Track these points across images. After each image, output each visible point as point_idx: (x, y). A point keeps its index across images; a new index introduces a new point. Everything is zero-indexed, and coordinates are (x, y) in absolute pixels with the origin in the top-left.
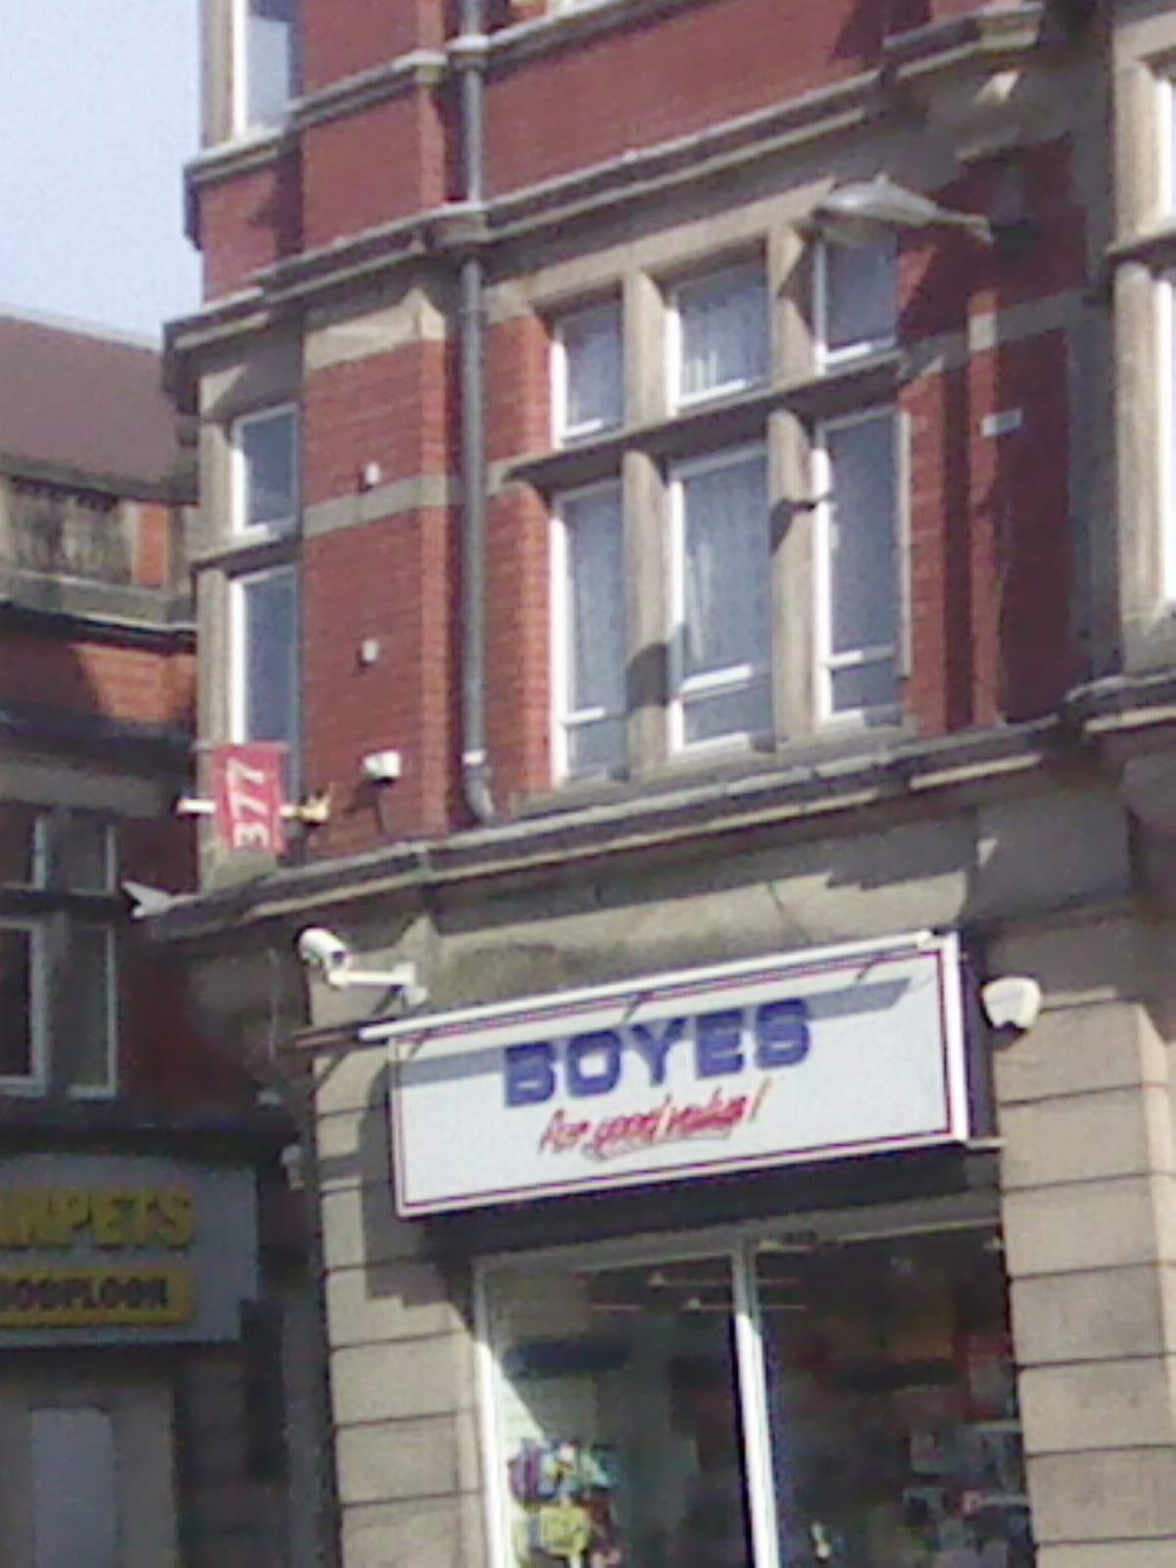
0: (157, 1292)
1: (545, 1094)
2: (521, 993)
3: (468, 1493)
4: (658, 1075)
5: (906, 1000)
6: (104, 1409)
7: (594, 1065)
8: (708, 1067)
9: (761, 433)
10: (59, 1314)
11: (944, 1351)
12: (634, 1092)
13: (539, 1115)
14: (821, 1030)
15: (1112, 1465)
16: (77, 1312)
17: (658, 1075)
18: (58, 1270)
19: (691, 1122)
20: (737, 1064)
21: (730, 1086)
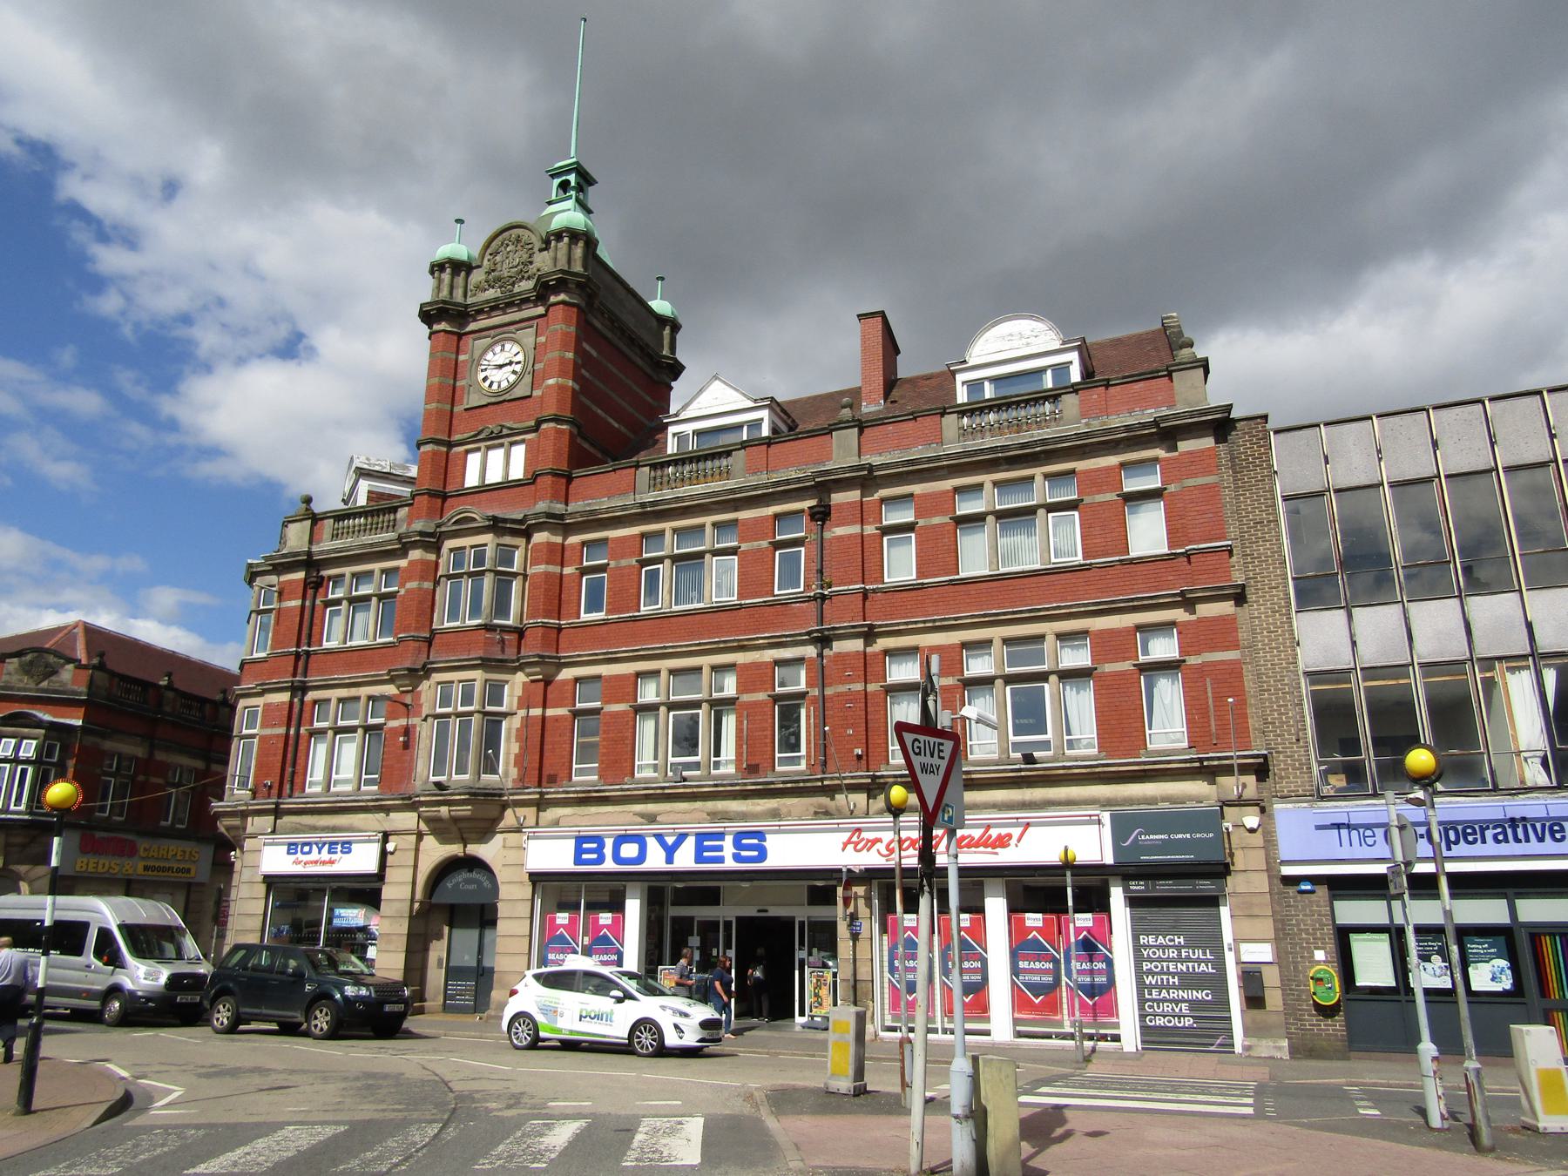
0: (188, 871)
1: (296, 853)
2: (293, 833)
3: (465, 847)
4: (320, 853)
5: (340, 615)
6: (171, 894)
7: (306, 849)
8: (329, 852)
9: (370, 600)
10: (166, 874)
11: (424, 772)
12: (315, 855)
13: (293, 857)
14: (354, 846)
15: (394, 937)
16: (170, 874)
17: (320, 853)
18: (167, 865)
19: (324, 863)
20: (336, 853)
21: (334, 857)
